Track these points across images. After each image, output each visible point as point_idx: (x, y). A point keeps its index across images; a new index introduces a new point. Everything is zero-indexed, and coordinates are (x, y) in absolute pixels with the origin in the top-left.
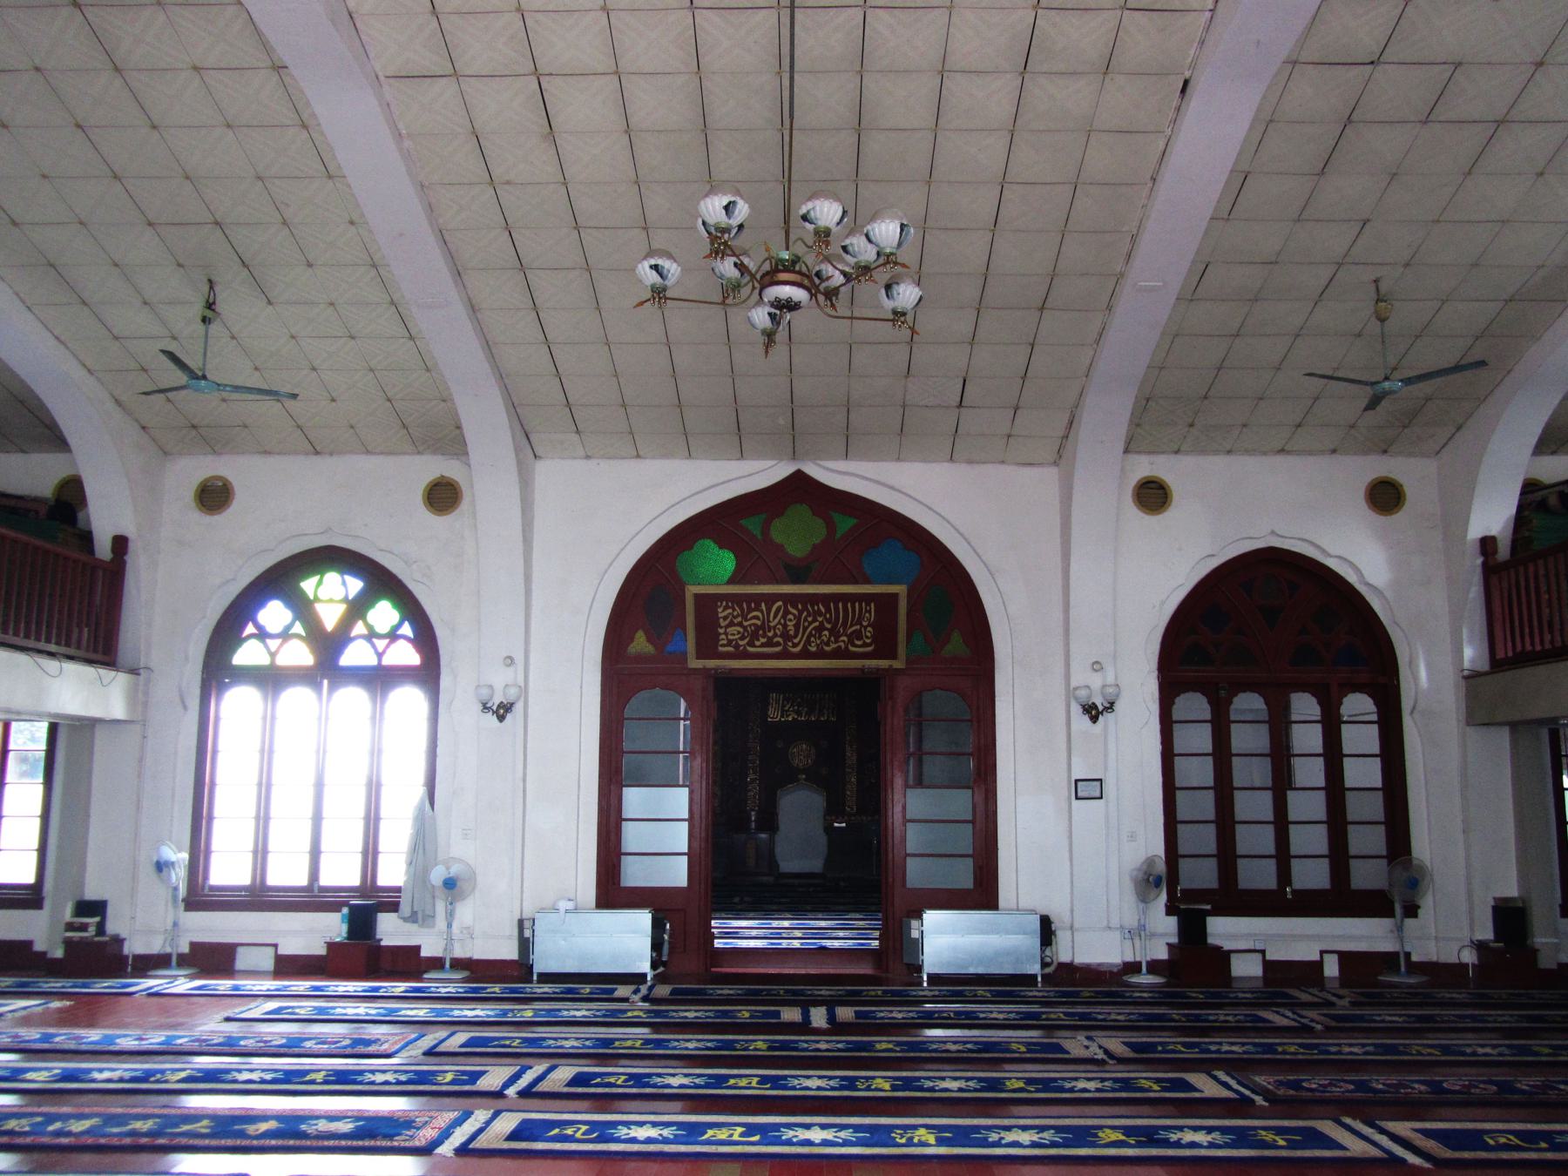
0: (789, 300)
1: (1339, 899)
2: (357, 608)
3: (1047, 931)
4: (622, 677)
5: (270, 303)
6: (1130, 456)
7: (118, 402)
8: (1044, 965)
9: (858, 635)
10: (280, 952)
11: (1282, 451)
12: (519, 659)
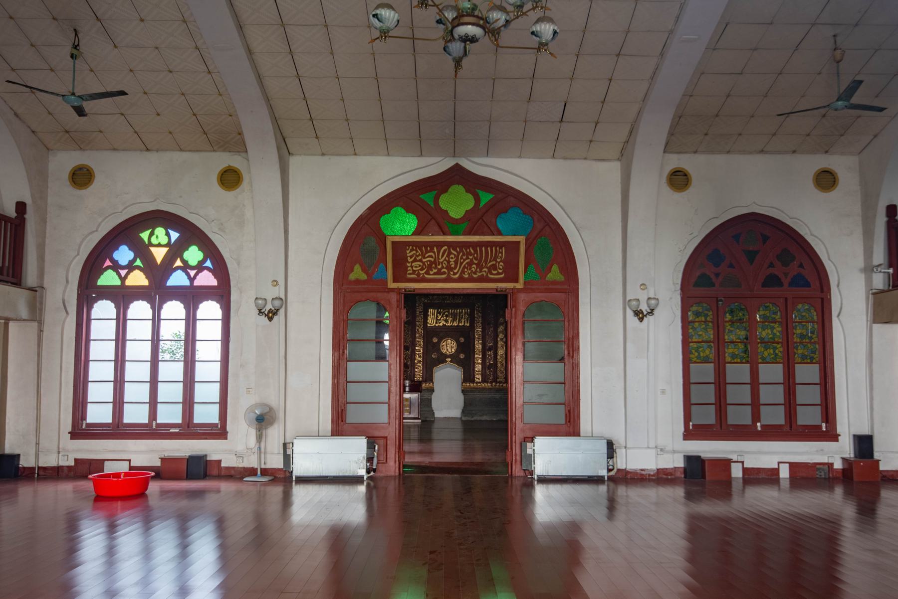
0: (467, 36)
1: (791, 430)
2: (176, 250)
3: (611, 447)
4: (348, 292)
5: (115, 46)
6: (667, 155)
7: (16, 114)
8: (609, 470)
9: (494, 267)
10: (132, 465)
11: (762, 151)
12: (282, 282)
